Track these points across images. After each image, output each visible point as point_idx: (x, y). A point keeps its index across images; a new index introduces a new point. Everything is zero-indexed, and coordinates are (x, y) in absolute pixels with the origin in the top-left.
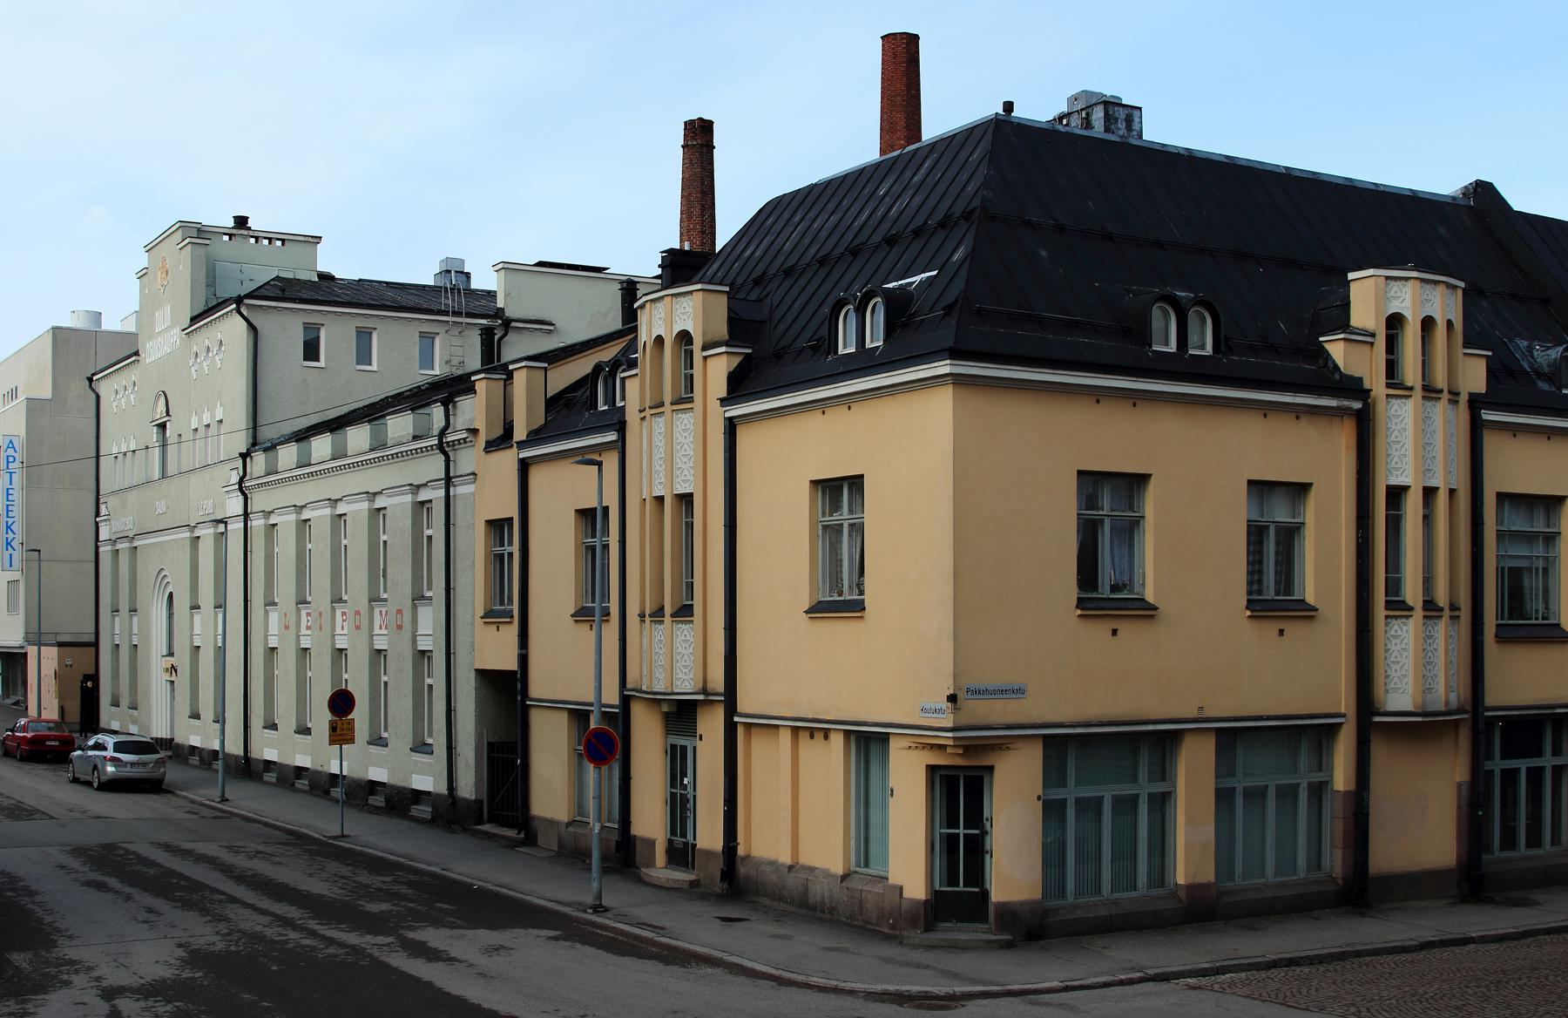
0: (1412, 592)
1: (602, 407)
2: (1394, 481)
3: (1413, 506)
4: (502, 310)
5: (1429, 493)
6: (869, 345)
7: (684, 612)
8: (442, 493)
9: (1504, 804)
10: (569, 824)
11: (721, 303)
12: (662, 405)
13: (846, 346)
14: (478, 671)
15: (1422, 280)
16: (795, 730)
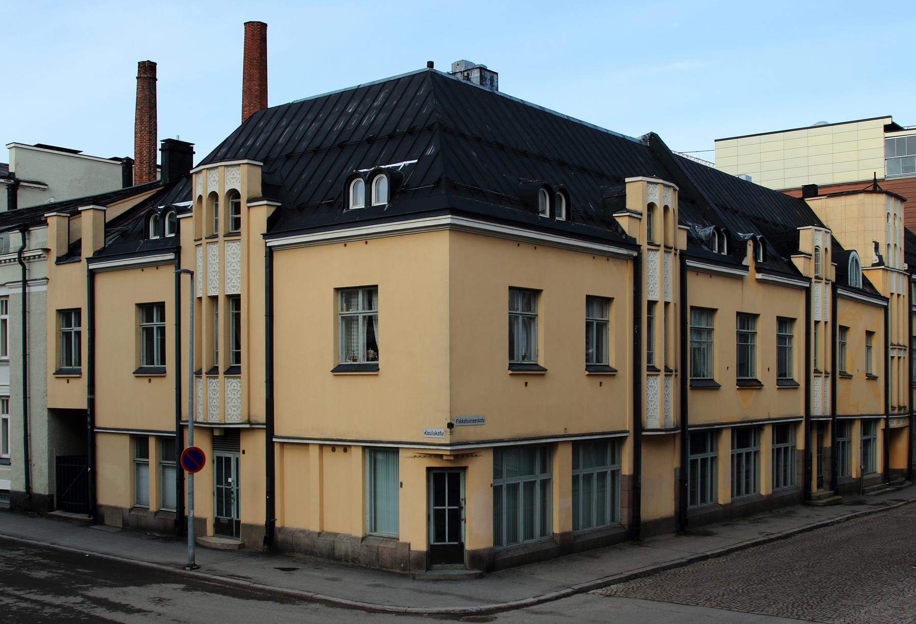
0: (658, 362)
1: (153, 237)
2: (652, 298)
3: (659, 311)
4: (13, 174)
5: (667, 304)
6: (374, 204)
7: (234, 371)
8: (20, 290)
9: (701, 478)
10: (131, 510)
11: (258, 173)
12: (216, 236)
13: (357, 201)
14: (49, 409)
15: (665, 185)
16: (321, 446)
